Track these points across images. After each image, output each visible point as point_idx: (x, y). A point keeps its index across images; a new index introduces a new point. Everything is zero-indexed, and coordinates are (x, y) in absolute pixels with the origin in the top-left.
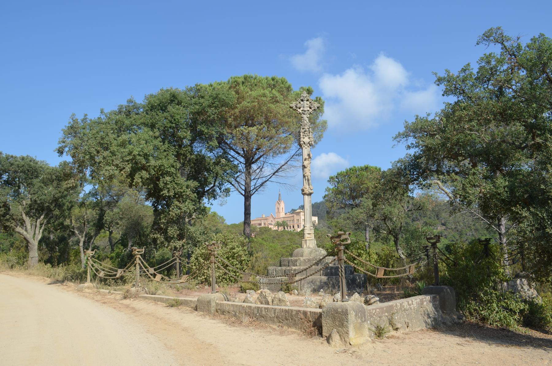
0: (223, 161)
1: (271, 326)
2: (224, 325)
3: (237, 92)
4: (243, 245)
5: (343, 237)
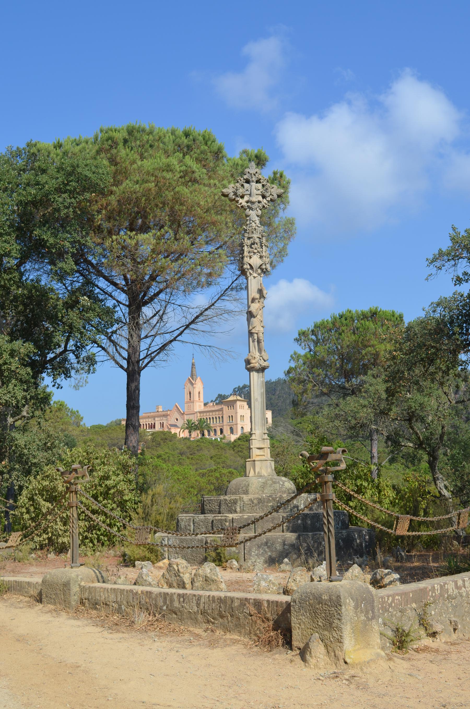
0: (84, 300)
1: (191, 629)
2: (99, 629)
3: (113, 161)
4: (125, 468)
5: (332, 458)
